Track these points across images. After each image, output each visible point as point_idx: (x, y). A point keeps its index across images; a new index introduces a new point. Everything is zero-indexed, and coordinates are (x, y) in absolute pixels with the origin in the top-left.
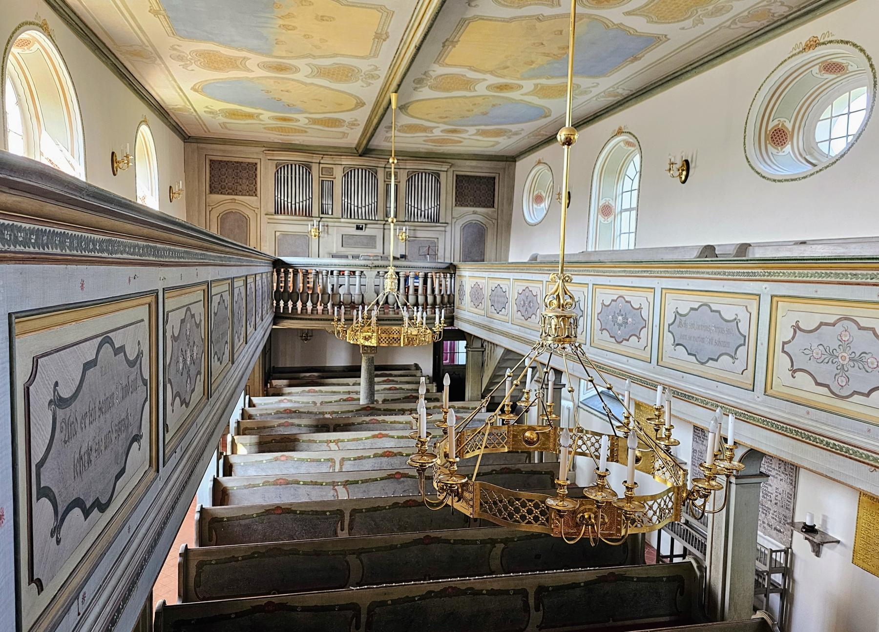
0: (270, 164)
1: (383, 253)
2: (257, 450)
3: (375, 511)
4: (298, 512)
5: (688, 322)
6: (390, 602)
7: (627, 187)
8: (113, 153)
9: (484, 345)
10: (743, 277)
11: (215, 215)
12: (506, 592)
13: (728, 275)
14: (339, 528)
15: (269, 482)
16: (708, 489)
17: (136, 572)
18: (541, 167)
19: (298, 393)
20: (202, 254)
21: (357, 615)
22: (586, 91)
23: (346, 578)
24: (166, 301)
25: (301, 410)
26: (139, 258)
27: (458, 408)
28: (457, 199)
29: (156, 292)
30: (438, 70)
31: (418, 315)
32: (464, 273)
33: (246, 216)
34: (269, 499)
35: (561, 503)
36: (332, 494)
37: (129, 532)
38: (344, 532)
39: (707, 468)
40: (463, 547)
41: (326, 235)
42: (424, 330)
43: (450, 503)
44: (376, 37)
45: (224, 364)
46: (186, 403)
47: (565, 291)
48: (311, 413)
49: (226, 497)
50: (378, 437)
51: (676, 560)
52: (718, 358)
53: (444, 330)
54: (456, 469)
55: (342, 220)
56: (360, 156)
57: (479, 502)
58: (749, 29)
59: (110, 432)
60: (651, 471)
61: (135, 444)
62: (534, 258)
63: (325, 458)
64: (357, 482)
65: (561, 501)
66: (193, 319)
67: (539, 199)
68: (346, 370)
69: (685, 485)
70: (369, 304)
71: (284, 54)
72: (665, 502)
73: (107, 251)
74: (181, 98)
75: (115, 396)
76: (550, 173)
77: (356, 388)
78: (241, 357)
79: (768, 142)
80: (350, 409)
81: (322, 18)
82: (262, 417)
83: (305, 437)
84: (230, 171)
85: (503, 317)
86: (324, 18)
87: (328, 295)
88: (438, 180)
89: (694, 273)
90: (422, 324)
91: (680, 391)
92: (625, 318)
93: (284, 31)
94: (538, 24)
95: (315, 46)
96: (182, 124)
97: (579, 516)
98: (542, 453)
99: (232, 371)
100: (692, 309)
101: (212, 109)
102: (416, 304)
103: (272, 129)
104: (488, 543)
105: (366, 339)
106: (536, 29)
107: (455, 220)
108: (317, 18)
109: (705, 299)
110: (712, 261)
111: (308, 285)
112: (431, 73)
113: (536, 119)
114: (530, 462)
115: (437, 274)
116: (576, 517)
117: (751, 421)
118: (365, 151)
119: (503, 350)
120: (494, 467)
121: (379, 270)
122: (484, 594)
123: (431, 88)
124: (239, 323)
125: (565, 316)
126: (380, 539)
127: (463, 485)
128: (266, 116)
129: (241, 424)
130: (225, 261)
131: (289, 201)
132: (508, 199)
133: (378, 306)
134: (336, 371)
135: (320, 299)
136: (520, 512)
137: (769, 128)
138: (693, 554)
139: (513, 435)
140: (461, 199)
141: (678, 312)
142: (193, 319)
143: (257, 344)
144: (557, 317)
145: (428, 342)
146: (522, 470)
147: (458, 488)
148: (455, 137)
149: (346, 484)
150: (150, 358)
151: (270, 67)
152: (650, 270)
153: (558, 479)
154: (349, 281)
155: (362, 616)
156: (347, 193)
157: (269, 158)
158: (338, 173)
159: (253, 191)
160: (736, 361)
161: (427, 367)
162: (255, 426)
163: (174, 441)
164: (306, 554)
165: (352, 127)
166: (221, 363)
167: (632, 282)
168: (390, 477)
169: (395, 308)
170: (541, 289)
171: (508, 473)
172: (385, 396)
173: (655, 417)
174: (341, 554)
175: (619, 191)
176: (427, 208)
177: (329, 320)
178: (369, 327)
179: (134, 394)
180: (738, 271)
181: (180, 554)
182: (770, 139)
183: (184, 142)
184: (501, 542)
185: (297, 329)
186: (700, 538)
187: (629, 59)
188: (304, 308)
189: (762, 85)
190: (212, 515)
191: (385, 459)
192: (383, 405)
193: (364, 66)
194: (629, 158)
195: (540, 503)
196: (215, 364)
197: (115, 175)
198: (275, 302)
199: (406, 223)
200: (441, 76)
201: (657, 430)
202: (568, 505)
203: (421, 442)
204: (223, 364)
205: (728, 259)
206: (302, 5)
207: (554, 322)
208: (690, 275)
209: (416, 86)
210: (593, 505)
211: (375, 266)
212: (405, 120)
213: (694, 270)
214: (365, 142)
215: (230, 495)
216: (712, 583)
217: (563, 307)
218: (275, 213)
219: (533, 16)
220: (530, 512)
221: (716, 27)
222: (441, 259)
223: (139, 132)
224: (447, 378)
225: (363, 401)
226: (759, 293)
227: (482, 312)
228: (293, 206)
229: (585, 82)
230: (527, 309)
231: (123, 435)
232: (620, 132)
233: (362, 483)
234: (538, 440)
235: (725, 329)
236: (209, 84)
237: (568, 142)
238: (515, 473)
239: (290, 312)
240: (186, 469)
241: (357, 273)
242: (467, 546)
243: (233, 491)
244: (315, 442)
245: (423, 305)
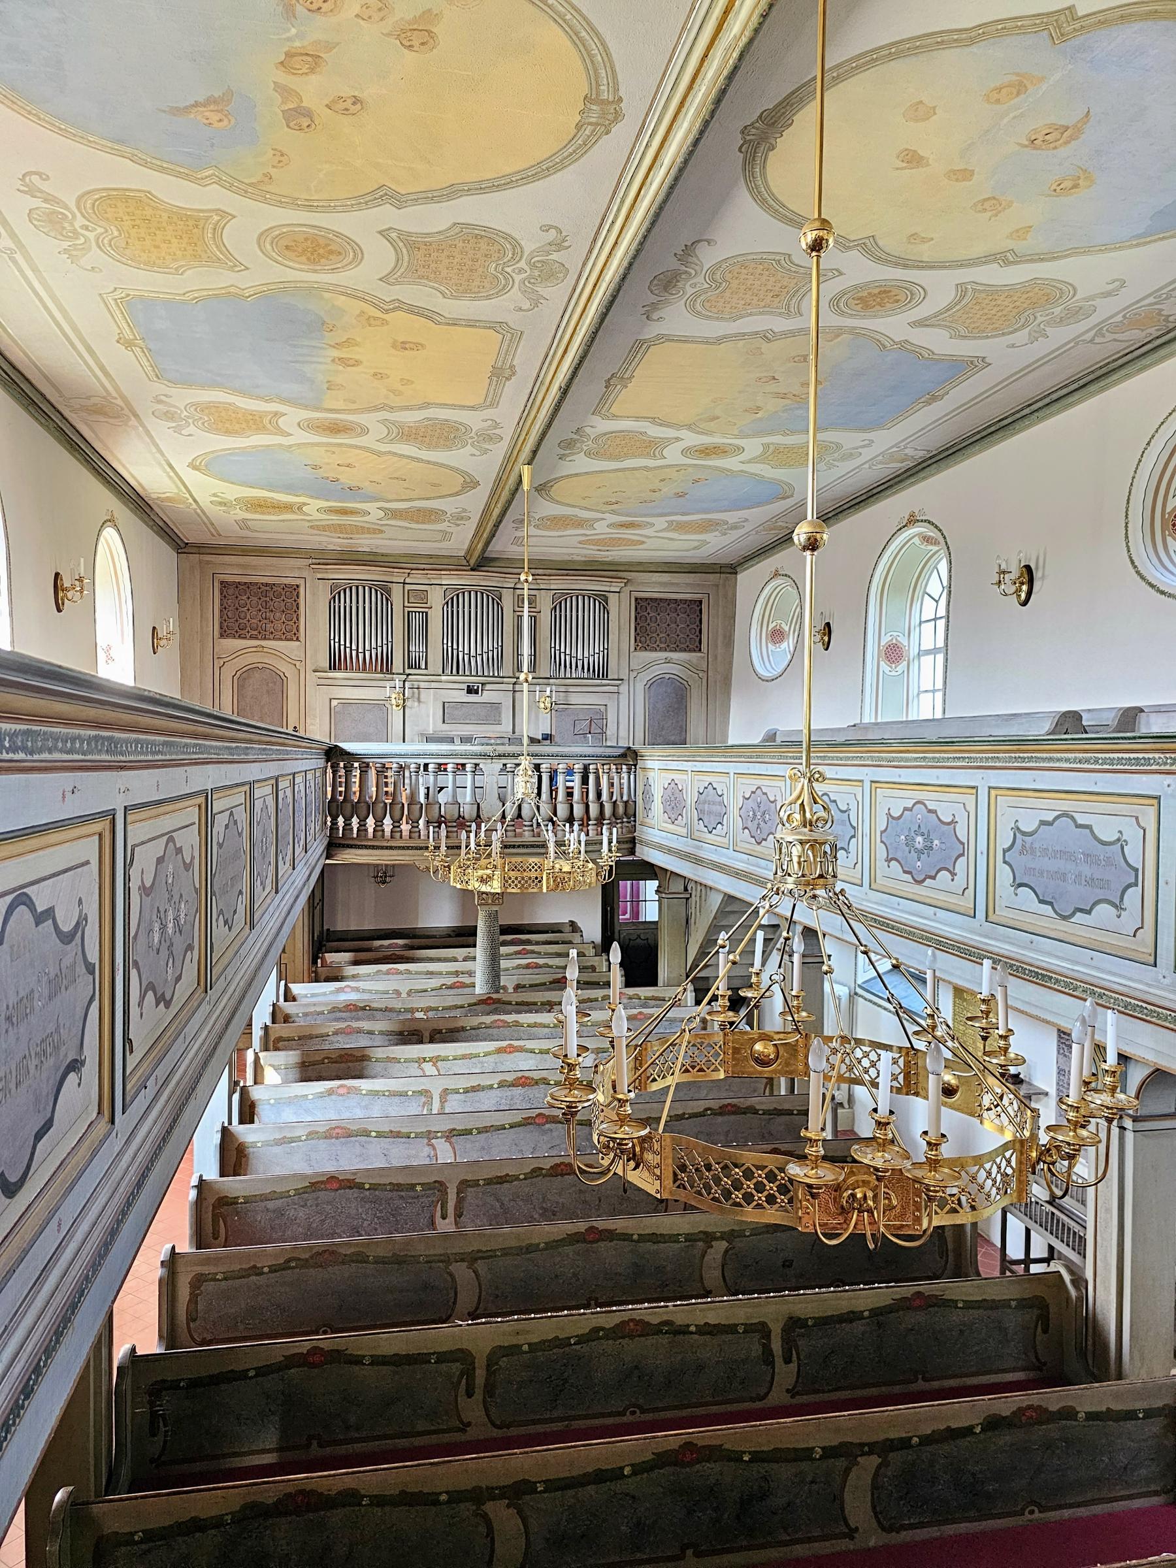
1: (514, 733)
2: (298, 1076)
3: (501, 1183)
5: (1036, 845)
6: (525, 1348)
7: (928, 613)
8: (57, 575)
9: (689, 888)
10: (1129, 767)
11: (228, 673)
12: (731, 1329)
13: (1102, 764)
14: (438, 1214)
15: (317, 1133)
16: (1074, 1145)
17: (69, 1301)
18: (779, 581)
19: (369, 975)
20: (196, 745)
21: (469, 1373)
22: (851, 454)
24: (129, 828)
25: (374, 1005)
26: (81, 757)
27: (646, 998)
28: (638, 638)
29: (112, 814)
30: (601, 425)
31: (574, 837)
32: (649, 764)
33: (282, 675)
34: (317, 1162)
35: (814, 1171)
36: (426, 1154)
37: (59, 1231)
38: (447, 1221)
39: (1072, 1106)
40: (655, 1247)
41: (416, 704)
42: (581, 863)
43: (620, 1172)
44: (493, 374)
45: (235, 930)
46: (164, 999)
47: (814, 798)
48: (391, 1010)
49: (244, 1160)
50: (506, 1052)
51: (1035, 1269)
52: (1091, 909)
53: (617, 862)
54: (630, 1112)
55: (444, 678)
56: (472, 570)
57: (671, 1169)
58: (1127, 344)
59: (25, 1057)
60: (977, 1113)
61: (72, 1076)
62: (771, 737)
63: (414, 1089)
64: (468, 1132)
65: (812, 1169)
66: (180, 855)
67: (777, 636)
68: (452, 934)
69: (1034, 1136)
70: (490, 819)
71: (340, 405)
72: (999, 1167)
73: (24, 749)
74: (174, 482)
75: (36, 995)
76: (795, 591)
77: (468, 965)
78: (267, 916)
79: (1167, 533)
80: (459, 1003)
81: (404, 346)
82: (308, 1018)
83: (380, 1053)
85: (719, 839)
86: (407, 346)
87: (419, 806)
88: (604, 608)
89: (1044, 760)
90: (580, 852)
91: (1028, 967)
92: (928, 838)
93: (341, 368)
94: (765, 346)
95: (393, 392)
96: (175, 525)
97: (845, 1195)
98: (793, 1080)
99: (250, 941)
100: (1043, 823)
101: (222, 498)
102: (570, 820)
103: (324, 528)
104: (699, 1240)
105: (483, 880)
106: (762, 353)
107: (635, 674)
108: (394, 346)
109: (1066, 805)
110: (1073, 739)
111: (385, 789)
112: (588, 430)
113: (769, 502)
114: (772, 1094)
115: (605, 767)
116: (841, 1196)
117: (1153, 1020)
118: (482, 562)
119: (721, 896)
120: (708, 1104)
121: (505, 761)
122: (692, 1333)
123: (588, 454)
124: (264, 858)
125: (816, 841)
126: (508, 1234)
127: (643, 1140)
128: (314, 507)
129: (271, 1032)
130: (238, 755)
131: (354, 647)
132: (725, 637)
133: (503, 823)
134: (434, 937)
135: (406, 812)
136: (742, 1188)
137: (1168, 510)
138: (1066, 1259)
139: (734, 1048)
140: (644, 637)
141: (1018, 829)
142: (180, 855)
143: (295, 893)
144: (802, 843)
145: (590, 883)
146: (757, 1107)
147: (634, 1146)
148: (629, 534)
149: (451, 1135)
150: (100, 927)
151: (318, 427)
152: (969, 755)
153: (807, 1129)
154: (454, 780)
155: (478, 1372)
156: (451, 630)
157: (319, 576)
158: (436, 598)
160: (1123, 913)
161: (592, 929)
162: (295, 1035)
163: (145, 1065)
164: (379, 1261)
165: (459, 522)
166: (230, 929)
167: (938, 777)
168: (526, 1122)
169: (535, 826)
171: (734, 1113)
172: (518, 979)
173: (980, 1015)
174: (442, 1261)
175: (915, 621)
176: (586, 655)
177: (421, 848)
178: (488, 861)
179: (71, 989)
180: (1120, 755)
181: (162, 1262)
182: (1171, 527)
184: (722, 1238)
185: (368, 865)
186: (1077, 1228)
187: (923, 400)
188: (380, 828)
189: (1153, 436)
190: (218, 1193)
191: (519, 1091)
192: (515, 995)
193: (475, 421)
194: (929, 564)
195: (777, 1172)
196: (219, 930)
197: (59, 610)
198: (329, 819)
199: (551, 681)
200: (605, 434)
201: (985, 1039)
202: (827, 1174)
203: (569, 1065)
204: (233, 929)
205: (1101, 736)
206: (370, 325)
207: (796, 851)
208: (1038, 765)
209: (563, 452)
210: (870, 1174)
211: (499, 756)
212: (547, 509)
213: (1044, 755)
214: (480, 546)
215: (251, 1156)
216: (1098, 1310)
217: (811, 825)
219: (757, 333)
220: (760, 1187)
221: (1069, 342)
222: (611, 741)
223: (102, 539)
224: (615, 950)
225: (480, 989)
226: (1158, 794)
227: (684, 831)
228: (361, 656)
229: (849, 439)
230: (759, 824)
231: (51, 1061)
232: (912, 521)
233: (479, 1133)
234: (777, 1057)
235: (1102, 857)
236: (218, 456)
237: (812, 545)
238: (744, 1113)
239: (355, 836)
240: (164, 1117)
241: (469, 767)
242: (662, 1245)
244: (397, 1060)
245: (582, 820)
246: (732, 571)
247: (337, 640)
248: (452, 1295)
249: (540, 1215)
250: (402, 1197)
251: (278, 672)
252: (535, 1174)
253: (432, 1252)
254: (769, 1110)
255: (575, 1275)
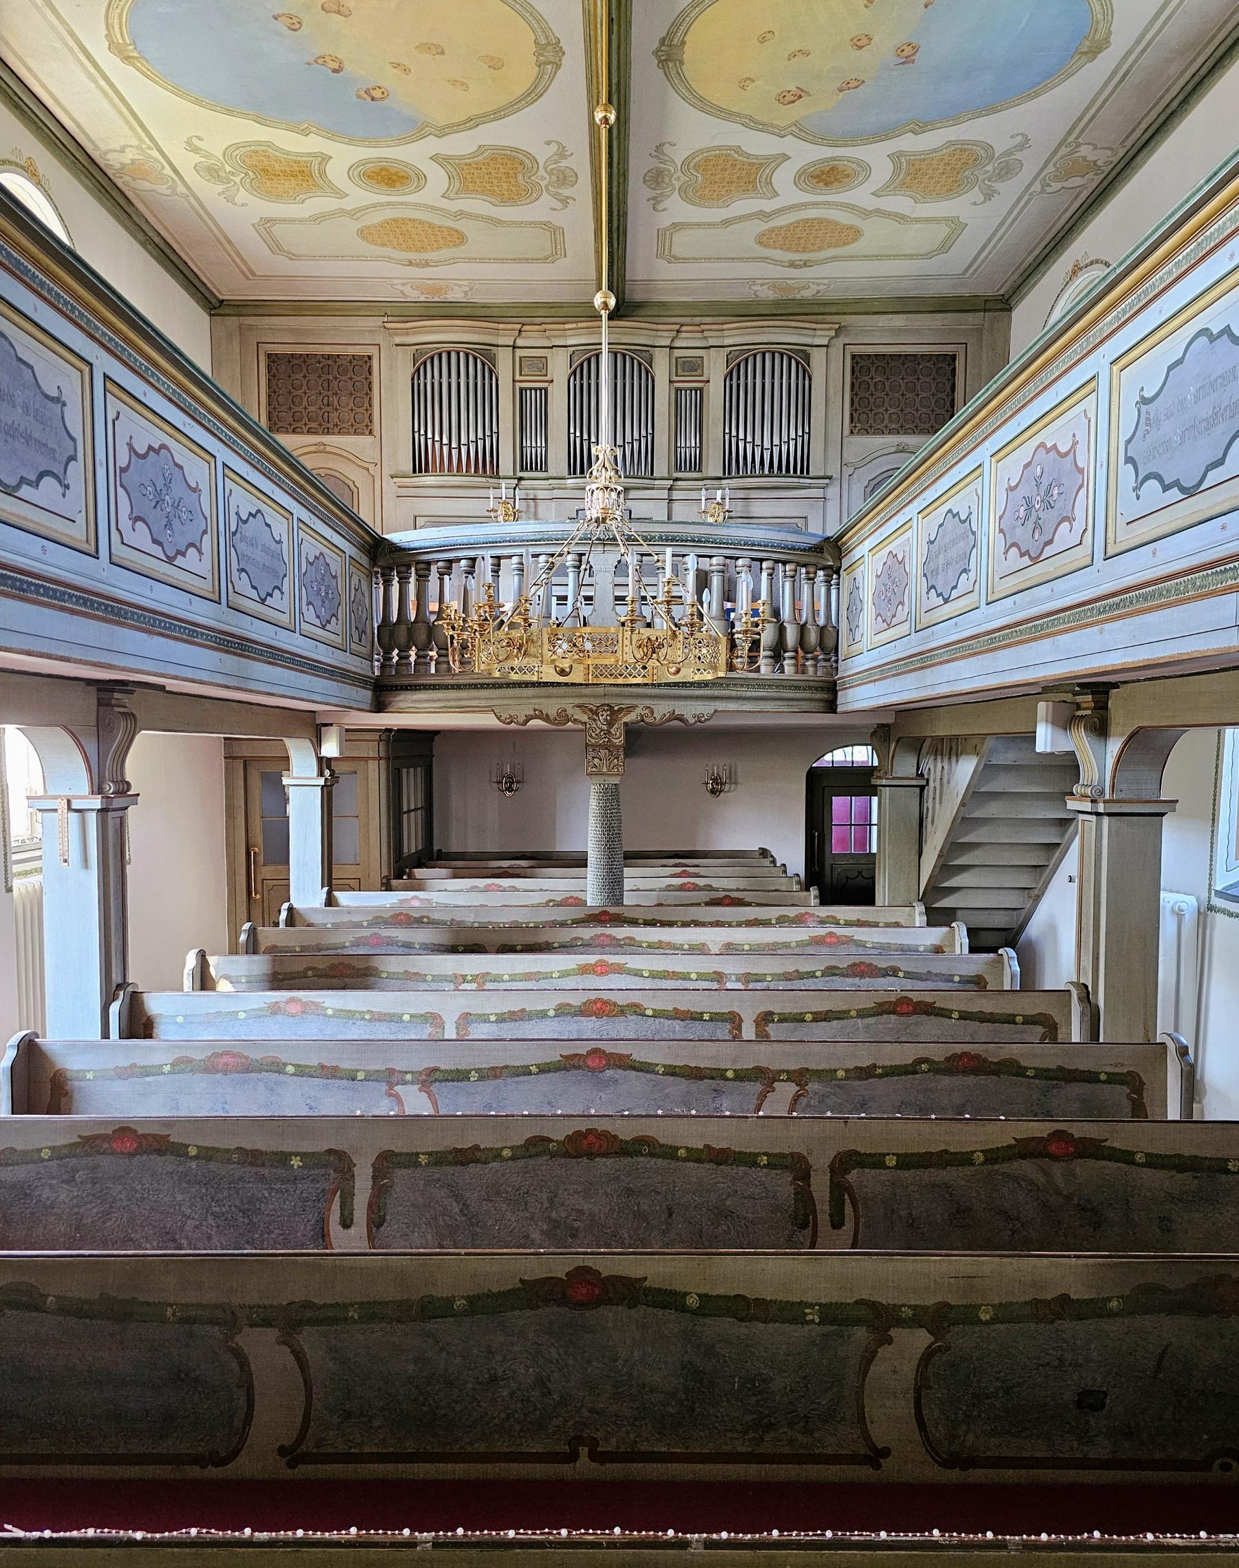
0: (400, 355)
4: (193, 1151)
15: (190, 1061)
23: (237, 1423)
38: (352, 1231)
40: (743, 1329)
49: (64, 1100)
50: (595, 972)
84: (313, 377)
88: (804, 371)
104: (857, 1322)
149: (431, 1078)
157: (398, 340)
159: (363, 425)
170: (1092, 417)
171: (975, 1072)
172: (658, 896)
174: (213, 1322)
183: (211, 315)
215: (76, 1094)
218: (414, 472)
228: (455, 452)
233: (481, 1078)
238: (996, 1073)
242: (761, 1326)
243: (83, 1084)
246: (1002, 306)
247: (422, 432)
248: (242, 1401)
249: (543, 1232)
250: (262, 1178)
251: (347, 481)
252: (533, 1151)
253: (192, 1297)
254: (1047, 1070)
255: (541, 1382)
